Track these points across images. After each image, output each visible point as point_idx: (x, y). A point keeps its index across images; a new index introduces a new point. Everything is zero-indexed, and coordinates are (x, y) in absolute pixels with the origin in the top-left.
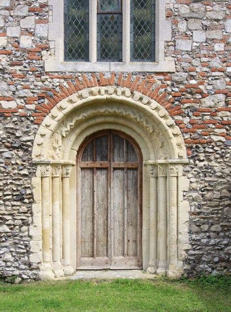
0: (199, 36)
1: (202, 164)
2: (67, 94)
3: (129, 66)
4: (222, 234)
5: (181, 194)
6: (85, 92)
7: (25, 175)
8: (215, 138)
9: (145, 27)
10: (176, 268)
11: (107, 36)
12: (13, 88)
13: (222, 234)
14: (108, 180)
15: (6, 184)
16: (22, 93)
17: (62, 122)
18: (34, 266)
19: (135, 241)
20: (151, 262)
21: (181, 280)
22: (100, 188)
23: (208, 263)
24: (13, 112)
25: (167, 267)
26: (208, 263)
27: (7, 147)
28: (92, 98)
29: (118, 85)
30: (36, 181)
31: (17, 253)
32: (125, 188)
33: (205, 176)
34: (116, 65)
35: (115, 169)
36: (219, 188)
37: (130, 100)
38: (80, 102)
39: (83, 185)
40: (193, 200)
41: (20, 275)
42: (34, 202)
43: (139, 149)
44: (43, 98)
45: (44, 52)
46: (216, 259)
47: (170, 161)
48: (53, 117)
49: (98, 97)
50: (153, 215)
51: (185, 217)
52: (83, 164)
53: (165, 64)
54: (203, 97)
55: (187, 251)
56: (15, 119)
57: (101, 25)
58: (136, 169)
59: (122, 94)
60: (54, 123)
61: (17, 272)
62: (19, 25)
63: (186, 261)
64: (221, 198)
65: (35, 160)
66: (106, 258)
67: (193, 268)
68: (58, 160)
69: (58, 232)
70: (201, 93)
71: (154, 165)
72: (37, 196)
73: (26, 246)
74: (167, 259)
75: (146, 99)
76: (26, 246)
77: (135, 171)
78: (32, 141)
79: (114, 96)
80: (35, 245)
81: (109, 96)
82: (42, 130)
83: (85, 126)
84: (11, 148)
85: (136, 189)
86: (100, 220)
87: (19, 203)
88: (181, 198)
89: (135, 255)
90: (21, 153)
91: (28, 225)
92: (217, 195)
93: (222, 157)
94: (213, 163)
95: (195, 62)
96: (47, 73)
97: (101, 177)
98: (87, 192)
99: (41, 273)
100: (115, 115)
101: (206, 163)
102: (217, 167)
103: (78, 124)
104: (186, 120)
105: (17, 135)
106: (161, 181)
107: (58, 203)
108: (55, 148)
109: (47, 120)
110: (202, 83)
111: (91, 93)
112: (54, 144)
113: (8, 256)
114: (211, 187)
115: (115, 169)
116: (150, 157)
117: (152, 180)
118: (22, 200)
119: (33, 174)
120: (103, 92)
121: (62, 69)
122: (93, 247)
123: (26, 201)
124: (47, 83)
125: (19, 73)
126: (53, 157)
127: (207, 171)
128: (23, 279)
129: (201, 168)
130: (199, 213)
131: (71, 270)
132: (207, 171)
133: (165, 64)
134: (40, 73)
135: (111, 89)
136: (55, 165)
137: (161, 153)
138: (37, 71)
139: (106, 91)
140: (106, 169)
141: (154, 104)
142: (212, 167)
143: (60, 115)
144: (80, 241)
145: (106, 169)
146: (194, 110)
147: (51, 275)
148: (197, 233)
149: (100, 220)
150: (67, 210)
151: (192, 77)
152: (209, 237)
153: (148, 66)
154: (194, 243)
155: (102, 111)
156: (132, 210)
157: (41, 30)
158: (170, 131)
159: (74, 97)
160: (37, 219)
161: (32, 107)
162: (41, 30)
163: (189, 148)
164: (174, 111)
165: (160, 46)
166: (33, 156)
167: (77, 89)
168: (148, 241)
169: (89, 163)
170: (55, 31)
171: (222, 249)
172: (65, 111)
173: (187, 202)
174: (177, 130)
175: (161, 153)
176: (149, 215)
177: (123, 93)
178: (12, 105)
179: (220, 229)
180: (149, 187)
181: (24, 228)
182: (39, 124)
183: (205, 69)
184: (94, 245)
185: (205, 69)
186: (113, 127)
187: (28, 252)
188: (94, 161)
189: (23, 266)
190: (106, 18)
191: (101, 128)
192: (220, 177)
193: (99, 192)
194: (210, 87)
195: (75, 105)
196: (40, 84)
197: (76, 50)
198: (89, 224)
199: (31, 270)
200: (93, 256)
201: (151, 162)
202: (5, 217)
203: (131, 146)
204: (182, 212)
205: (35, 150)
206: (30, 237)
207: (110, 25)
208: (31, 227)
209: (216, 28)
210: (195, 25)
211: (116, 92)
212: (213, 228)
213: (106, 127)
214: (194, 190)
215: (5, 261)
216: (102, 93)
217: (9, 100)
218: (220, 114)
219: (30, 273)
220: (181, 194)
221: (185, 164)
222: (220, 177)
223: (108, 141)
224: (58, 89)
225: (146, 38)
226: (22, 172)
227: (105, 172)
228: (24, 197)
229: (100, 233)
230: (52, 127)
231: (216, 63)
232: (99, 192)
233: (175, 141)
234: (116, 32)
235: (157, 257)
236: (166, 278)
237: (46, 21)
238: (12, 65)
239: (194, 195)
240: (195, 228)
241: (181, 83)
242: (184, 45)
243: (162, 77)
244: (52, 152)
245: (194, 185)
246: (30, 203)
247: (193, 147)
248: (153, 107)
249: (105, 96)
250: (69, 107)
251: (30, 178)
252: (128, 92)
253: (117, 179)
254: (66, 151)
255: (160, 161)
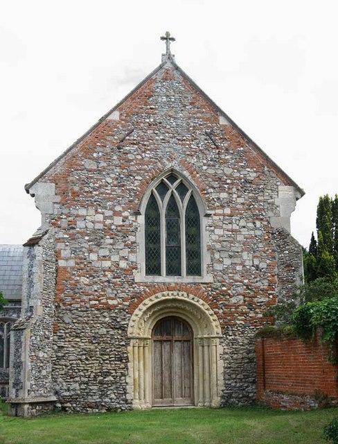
0: (227, 262)
1: (230, 338)
2: (148, 295)
3: (186, 279)
4: (243, 380)
5: (218, 355)
6: (159, 295)
7: (123, 345)
8: (238, 322)
9: (194, 255)
10: (217, 401)
11: (171, 260)
12: (115, 292)
13: (243, 380)
15: (111, 351)
16: (121, 295)
17: (145, 313)
18: (129, 401)
19: (189, 388)
20: (201, 400)
21: (220, 408)
22: (166, 353)
23: (236, 398)
24: (115, 306)
25: (211, 402)
26: (236, 398)
27: (112, 328)
28: (164, 298)
29: (179, 291)
30: (130, 348)
31: (119, 393)
32: (182, 354)
33: (233, 345)
34: (178, 278)
35: (175, 341)
36: (241, 352)
37: (186, 299)
38: (156, 301)
39: (155, 352)
40: (226, 360)
41: (120, 408)
42: (128, 362)
43: (190, 326)
44: (134, 298)
45: (134, 271)
46: (241, 396)
47: (212, 336)
48: (140, 310)
49: (167, 297)
50: (201, 370)
51: (221, 370)
52: (159, 337)
53: (207, 278)
54: (231, 297)
55: (223, 391)
56: (116, 311)
58: (189, 341)
59: (182, 296)
60: (140, 313)
61: (118, 406)
62: (118, 254)
63: (222, 397)
64: (242, 358)
65: (129, 335)
66: (170, 399)
67: (227, 401)
68: (142, 336)
69: (142, 382)
70: (229, 295)
71: (202, 339)
72: (131, 358)
73: (124, 389)
74: (211, 397)
75: (196, 299)
76: (124, 389)
77: (189, 342)
78: (127, 324)
79: (177, 297)
80: (129, 388)
81: (174, 297)
82: (133, 317)
83: (157, 315)
84: (114, 328)
85: (189, 354)
86: (166, 374)
87: (119, 363)
88: (218, 358)
89: (190, 397)
90: (120, 332)
91: (125, 376)
92: (240, 356)
93: (243, 333)
94: (238, 337)
95: (225, 277)
96: (136, 283)
97: (167, 347)
98: (158, 356)
99: (133, 406)
100: (177, 308)
101: (233, 337)
103: (154, 313)
104: (221, 311)
105: (118, 320)
106: (206, 348)
107: (142, 362)
108: (140, 329)
109: (137, 312)
110: (229, 289)
111: (163, 295)
112: (139, 325)
113: (113, 396)
114: (236, 351)
115: (175, 341)
116: (199, 333)
117: (200, 348)
118: (121, 361)
119: (129, 344)
120: (170, 295)
121: (146, 281)
122: (162, 393)
123: (124, 361)
124: (136, 289)
125: (119, 283)
126: (139, 334)
127: (234, 342)
128: (122, 410)
129: (230, 340)
130: (229, 368)
131: (150, 406)
132: (234, 342)
133: (207, 278)
134: (132, 283)
135: (175, 293)
136: (140, 339)
137: (205, 331)
138: (302, 377)
139: (172, 294)
140: (170, 341)
141: (201, 301)
142: (236, 340)
143: (144, 308)
144: (154, 389)
145: (170, 341)
146: (225, 305)
147: (144, 406)
148: (229, 380)
149: (166, 374)
150: (147, 368)
151: (224, 286)
152: (236, 382)
153: (197, 279)
155: (169, 305)
156: (187, 368)
157: (132, 257)
158: (211, 318)
159: (153, 297)
160: (131, 370)
161: (127, 303)
162: (132, 257)
163: (223, 328)
164: (213, 305)
165: (204, 267)
166: (128, 333)
167: (155, 293)
168: (199, 385)
169: (159, 337)
170: (140, 258)
171: (244, 390)
172: (147, 306)
173: (222, 361)
174: (215, 317)
175: (205, 331)
176: (198, 370)
177: (182, 295)
178: (115, 302)
179: (242, 377)
180: (198, 352)
181: (123, 378)
182: (131, 314)
183: (231, 281)
184: (162, 391)
185: (231, 281)
186: (174, 315)
187: (125, 393)
188: (162, 335)
189: (122, 402)
190: (171, 249)
191: (167, 315)
192: (240, 345)
193: (166, 356)
194: (234, 292)
195: (153, 302)
196: (132, 289)
197: (153, 269)
198: (159, 377)
199: (127, 404)
200: (162, 398)
201: (199, 336)
203: (186, 327)
204: (219, 367)
205: (130, 330)
206: (127, 383)
207: (174, 254)
208: (127, 377)
209: (237, 257)
210: (225, 255)
211: (178, 294)
212: (238, 377)
213: (171, 315)
214: (227, 353)
215: (111, 399)
216: (170, 295)
217: (112, 299)
218: (240, 307)
219: (127, 406)
220: (218, 355)
221: (220, 338)
222: (242, 345)
223: (173, 324)
224: (143, 293)
225: (195, 261)
226: (121, 343)
227: (169, 343)
228: (123, 359)
229: (167, 382)
230: (140, 316)
231: (237, 277)
232: (166, 356)
233: (214, 324)
234: (177, 258)
235: (204, 397)
236: (210, 407)
237: (135, 252)
238: (114, 278)
239: (227, 356)
240: (227, 377)
241: (217, 289)
242: (218, 267)
243: (205, 286)
244: (138, 331)
245: (226, 351)
246: (126, 362)
247: (226, 327)
248: (200, 303)
249: (172, 297)
250: (150, 304)
251: (126, 347)
252: (186, 295)
253: (177, 346)
254: (146, 331)
255: (205, 336)
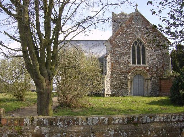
0: (152, 61)
3: (142, 65)
9: (144, 59)
14: (136, 92)
51: (150, 87)
53: (147, 65)
57: (137, 52)
102: (155, 80)
106: (147, 82)
109: (130, 73)
133: (147, 65)
134: (129, 66)
154: (152, 91)
170: (131, 60)
174: (149, 75)
178: (125, 71)
197: (134, 63)
202: (148, 90)
